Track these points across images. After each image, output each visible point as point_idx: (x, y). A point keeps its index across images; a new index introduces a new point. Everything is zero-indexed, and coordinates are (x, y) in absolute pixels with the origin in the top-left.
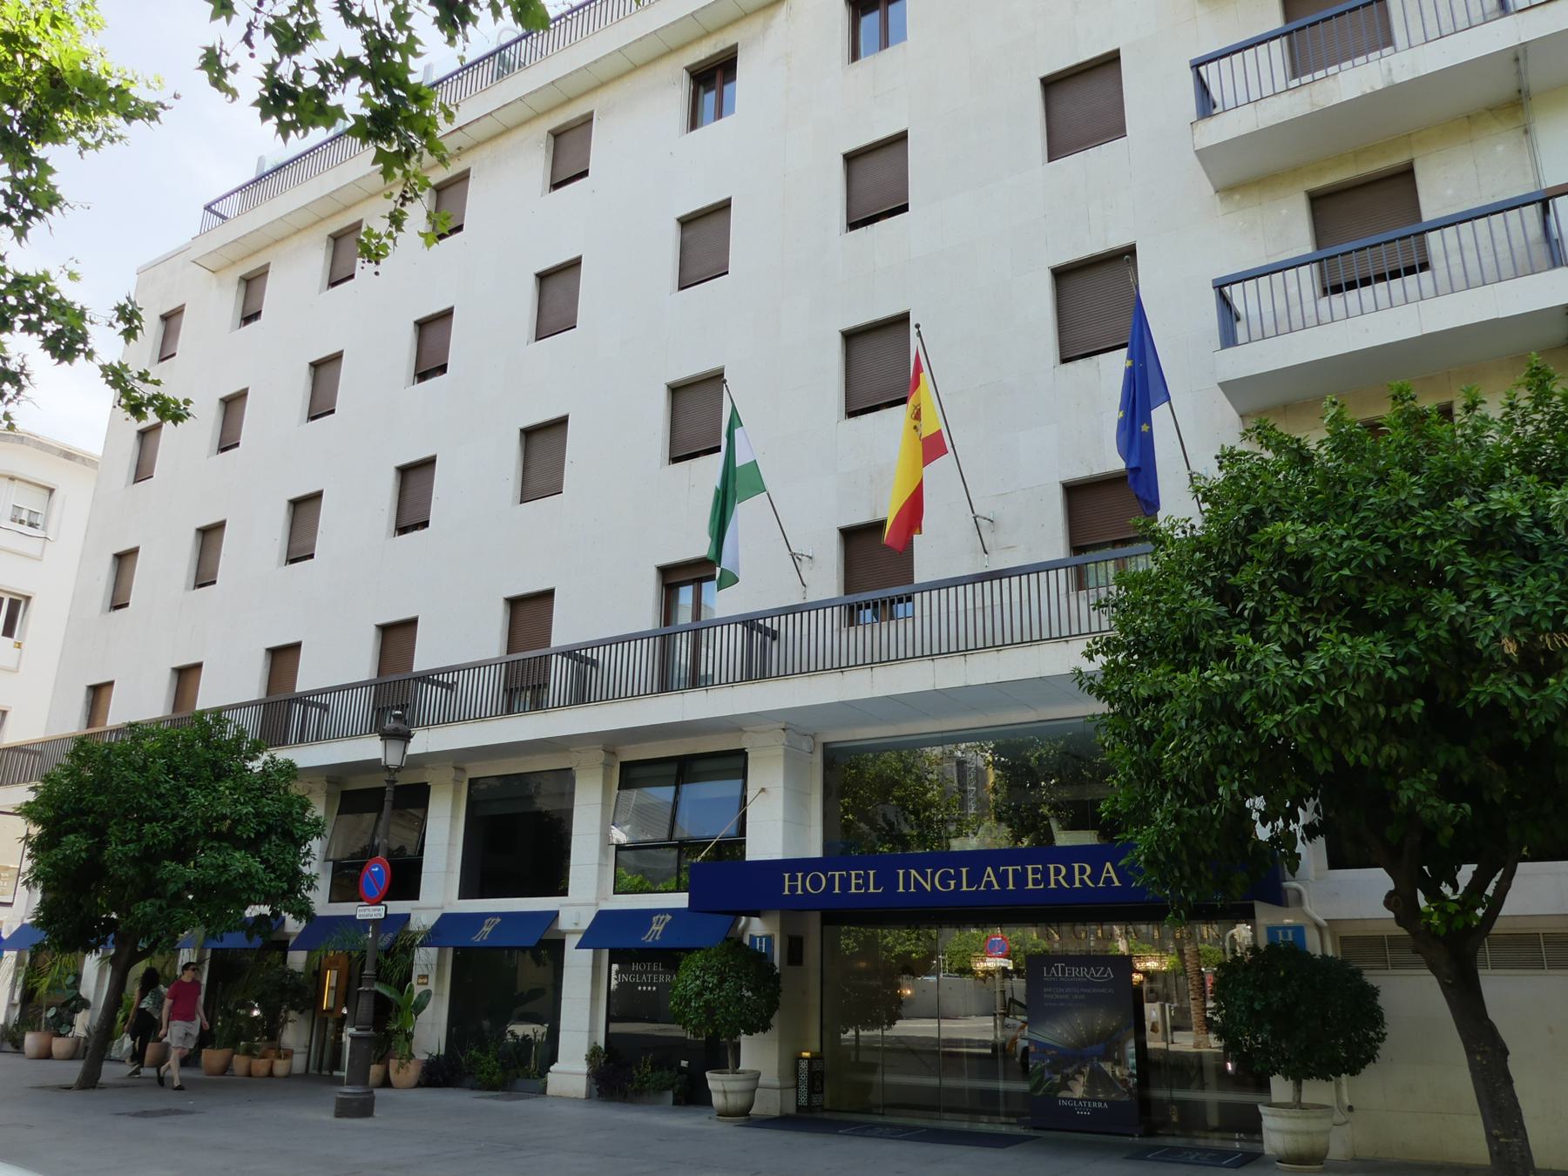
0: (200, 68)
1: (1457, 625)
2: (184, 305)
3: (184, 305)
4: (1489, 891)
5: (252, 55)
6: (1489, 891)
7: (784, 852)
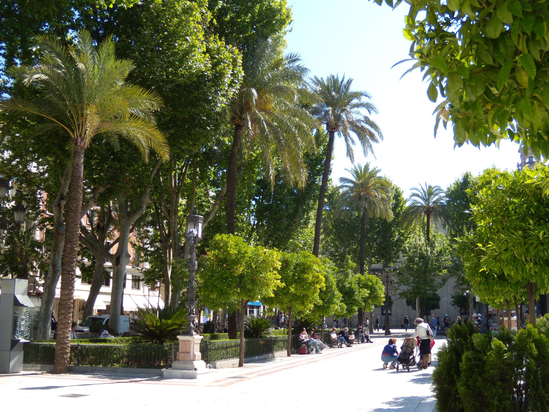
1: (133, 322)
4: (58, 293)
6: (58, 293)
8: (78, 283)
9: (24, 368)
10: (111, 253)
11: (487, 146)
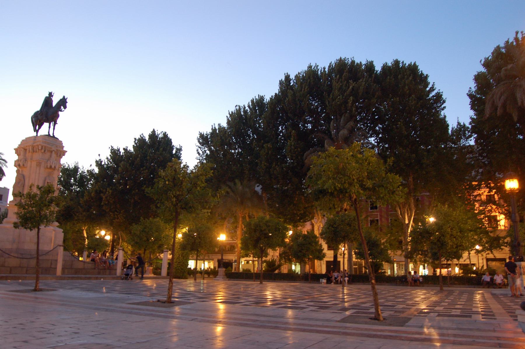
0: (14, 149)
2: (154, 130)
3: (154, 130)
4: (391, 291)
5: (434, 83)
8: (446, 270)
9: (330, 249)
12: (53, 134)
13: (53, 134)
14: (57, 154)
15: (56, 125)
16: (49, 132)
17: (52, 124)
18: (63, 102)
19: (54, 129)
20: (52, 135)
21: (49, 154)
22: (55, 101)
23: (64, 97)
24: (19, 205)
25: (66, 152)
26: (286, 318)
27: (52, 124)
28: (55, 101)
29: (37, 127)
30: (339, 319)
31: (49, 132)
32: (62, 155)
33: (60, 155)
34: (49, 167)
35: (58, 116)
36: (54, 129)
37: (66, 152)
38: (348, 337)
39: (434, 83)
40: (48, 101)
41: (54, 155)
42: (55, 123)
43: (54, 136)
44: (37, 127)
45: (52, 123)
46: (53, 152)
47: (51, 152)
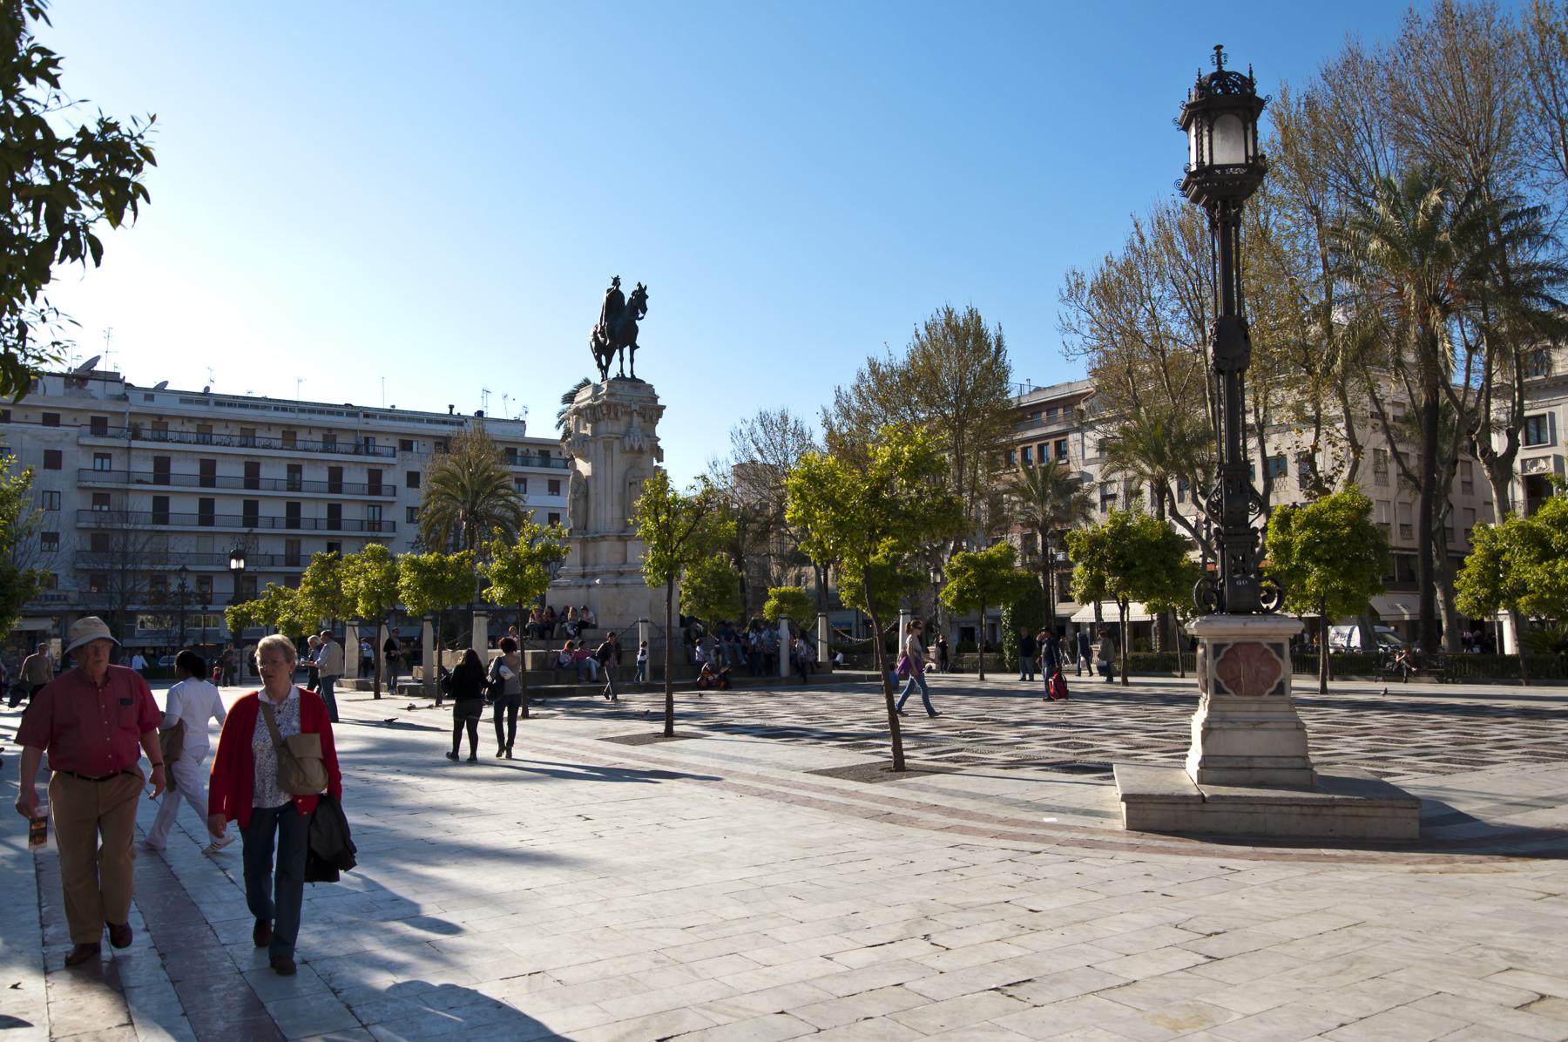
5: (1218, 48)
7: (352, 825)
9: (1211, 774)
10: (664, 728)
11: (660, 402)
12: (632, 372)
13: (632, 372)
14: (644, 417)
15: (636, 351)
16: (622, 371)
17: (627, 350)
18: (641, 295)
19: (632, 361)
20: (628, 375)
21: (625, 419)
22: (627, 291)
23: (639, 284)
24: (1157, 481)
25: (664, 407)
26: (414, 810)
27: (627, 350)
28: (627, 291)
29: (603, 358)
30: (312, 845)
31: (622, 371)
32: (654, 418)
33: (651, 418)
34: (627, 449)
35: (635, 330)
36: (632, 361)
37: (664, 407)
38: (1484, 721)
39: (1218, 48)
40: (614, 297)
41: (637, 420)
42: (634, 347)
43: (633, 376)
44: (603, 358)
45: (617, 353)
46: (635, 414)
47: (630, 414)
